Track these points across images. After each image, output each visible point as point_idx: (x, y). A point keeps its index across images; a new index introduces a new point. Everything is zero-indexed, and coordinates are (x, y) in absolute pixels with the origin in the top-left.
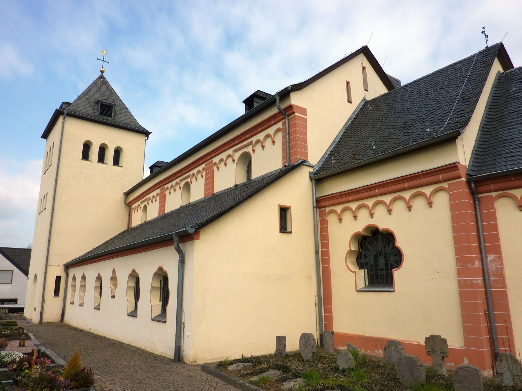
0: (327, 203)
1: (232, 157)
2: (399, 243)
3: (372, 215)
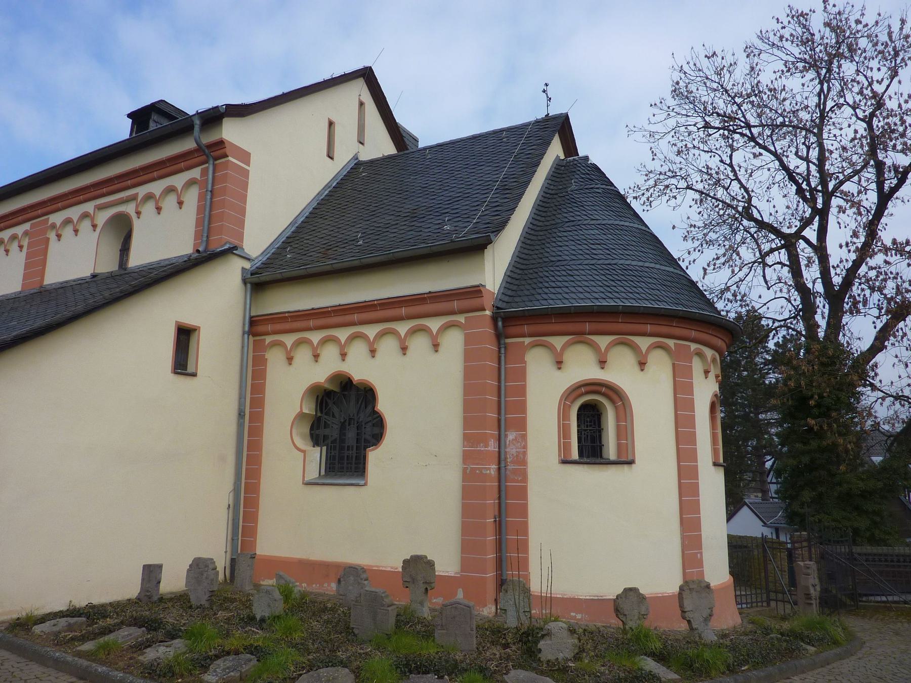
0: (270, 328)
1: (93, 219)
2: (383, 405)
3: (343, 355)
